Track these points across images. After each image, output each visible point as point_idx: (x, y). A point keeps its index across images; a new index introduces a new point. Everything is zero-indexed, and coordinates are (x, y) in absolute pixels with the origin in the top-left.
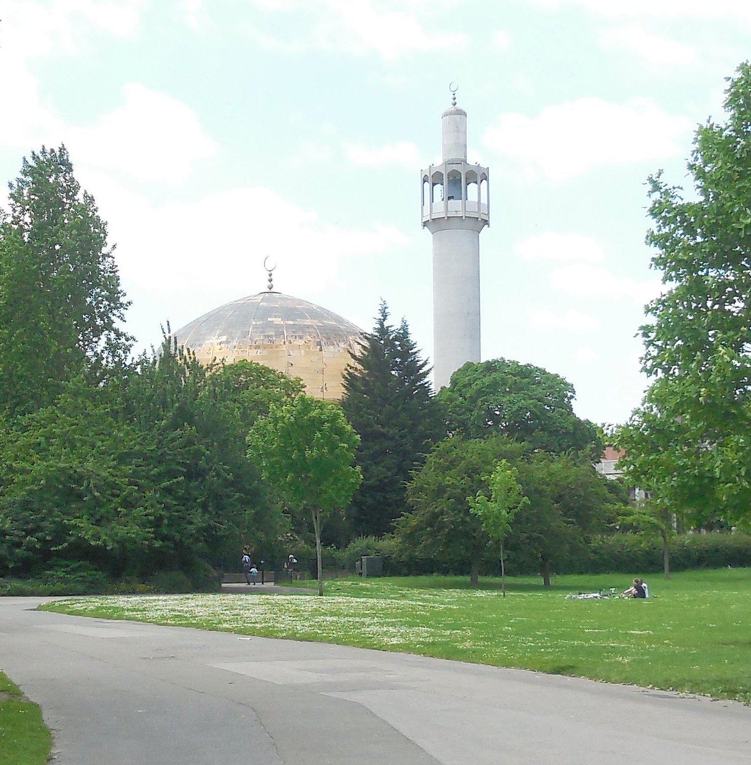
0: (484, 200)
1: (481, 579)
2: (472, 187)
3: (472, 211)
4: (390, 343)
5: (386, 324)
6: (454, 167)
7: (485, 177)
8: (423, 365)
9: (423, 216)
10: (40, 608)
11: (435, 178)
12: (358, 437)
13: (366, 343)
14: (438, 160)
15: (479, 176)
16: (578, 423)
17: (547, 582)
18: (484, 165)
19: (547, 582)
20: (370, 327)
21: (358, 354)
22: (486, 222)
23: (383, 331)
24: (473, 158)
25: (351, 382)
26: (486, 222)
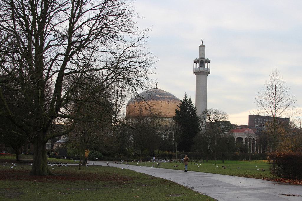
0: (209, 68)
1: (208, 161)
2: (206, 64)
3: (206, 70)
4: (187, 103)
5: (186, 99)
6: (202, 59)
7: (209, 62)
8: (194, 109)
9: (194, 71)
10: (250, 195)
11: (196, 61)
12: (272, 161)
13: (181, 103)
14: (198, 57)
15: (208, 62)
16: (232, 124)
17: (223, 162)
18: (209, 59)
19: (223, 162)
20: (182, 99)
21: (179, 105)
22: (209, 73)
23: (185, 100)
24: (206, 57)
25: (177, 112)
26: (209, 73)
